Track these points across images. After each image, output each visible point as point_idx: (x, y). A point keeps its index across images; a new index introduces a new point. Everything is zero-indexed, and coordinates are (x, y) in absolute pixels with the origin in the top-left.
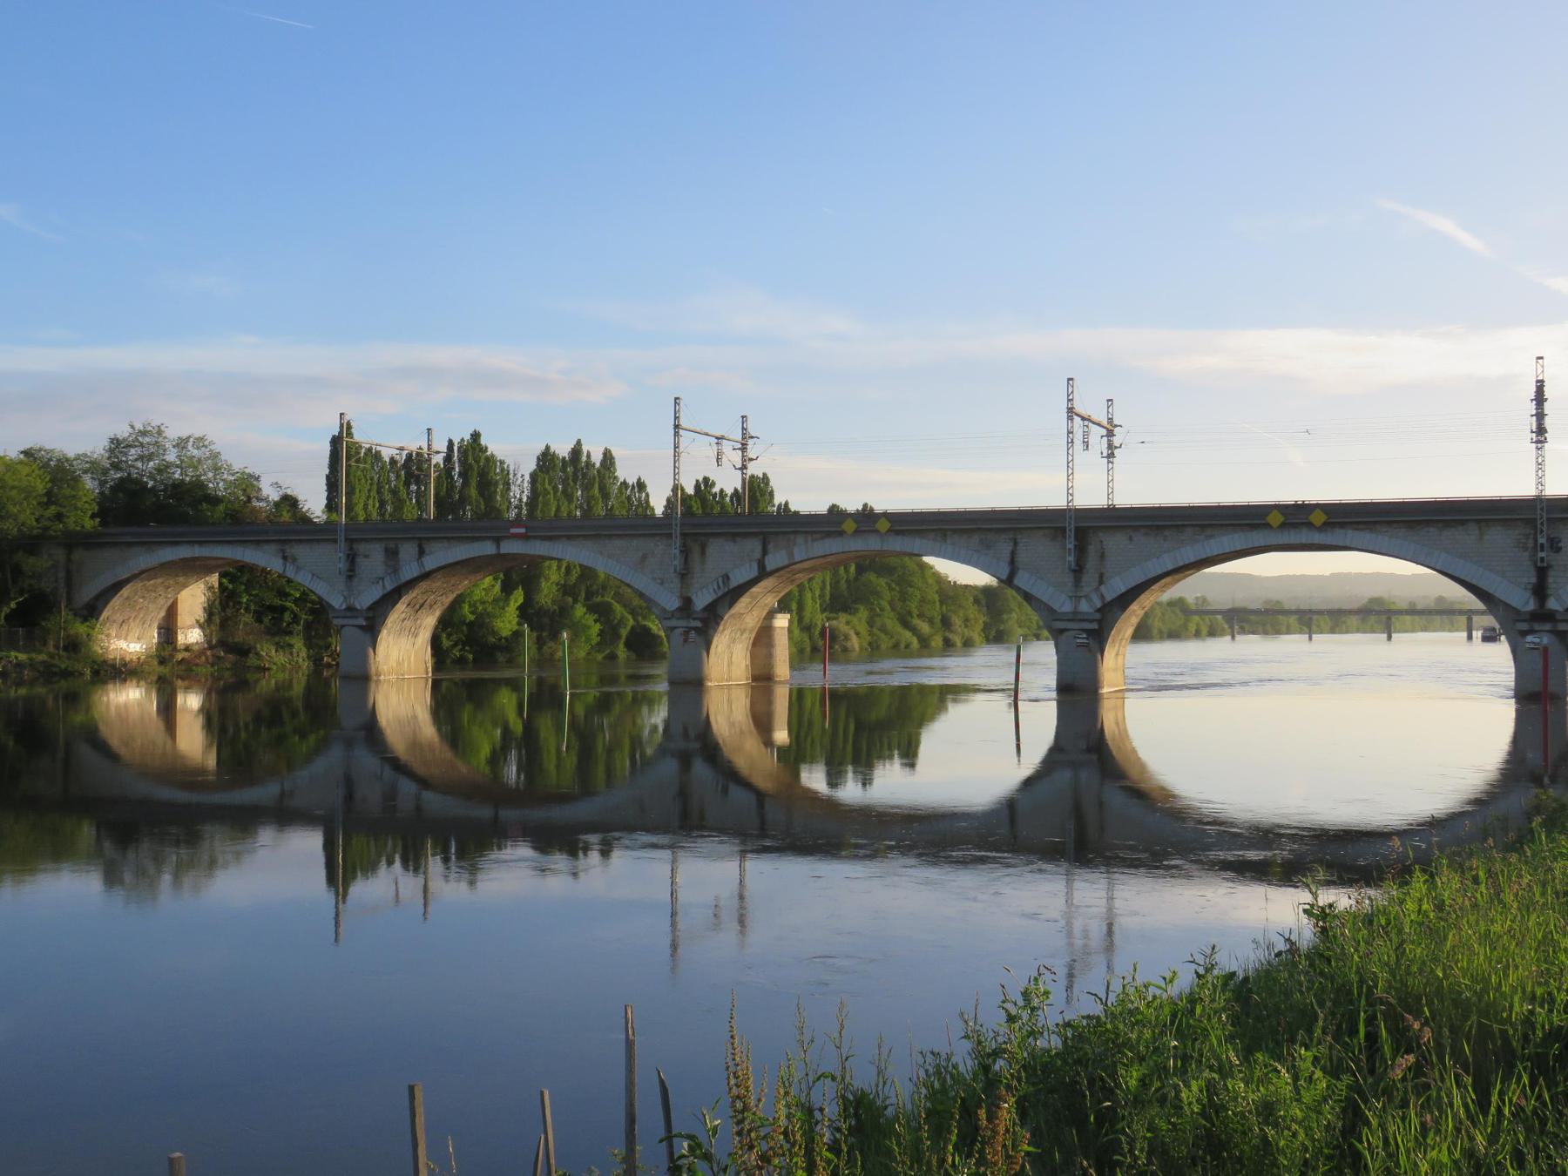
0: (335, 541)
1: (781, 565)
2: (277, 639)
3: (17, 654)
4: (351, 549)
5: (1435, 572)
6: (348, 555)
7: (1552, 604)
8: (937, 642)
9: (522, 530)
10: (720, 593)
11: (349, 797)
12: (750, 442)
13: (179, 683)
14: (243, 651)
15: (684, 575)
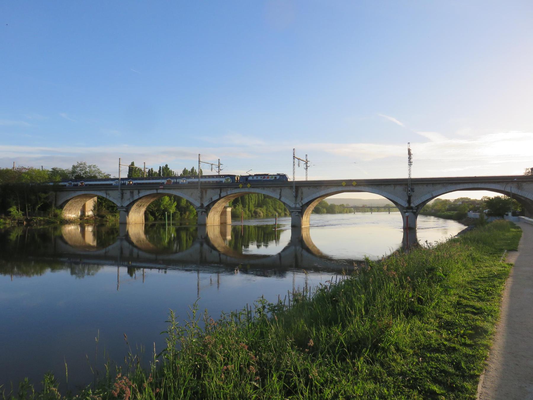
0: (118, 190)
1: (224, 195)
2: (112, 214)
3: (40, 218)
4: (122, 192)
5: (385, 198)
6: (121, 193)
7: (412, 205)
8: (283, 214)
9: (162, 187)
10: (210, 203)
11: (122, 253)
12: (221, 166)
13: (86, 224)
14: (103, 217)
15: (202, 198)
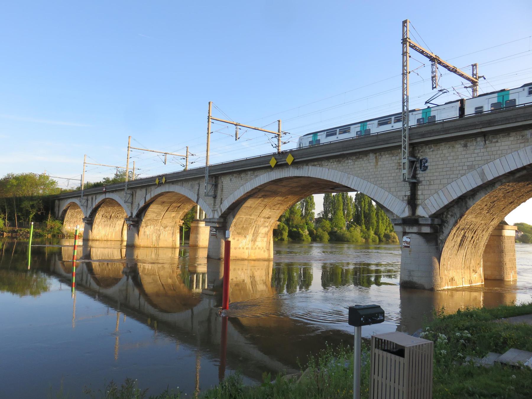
7: (420, 212)
